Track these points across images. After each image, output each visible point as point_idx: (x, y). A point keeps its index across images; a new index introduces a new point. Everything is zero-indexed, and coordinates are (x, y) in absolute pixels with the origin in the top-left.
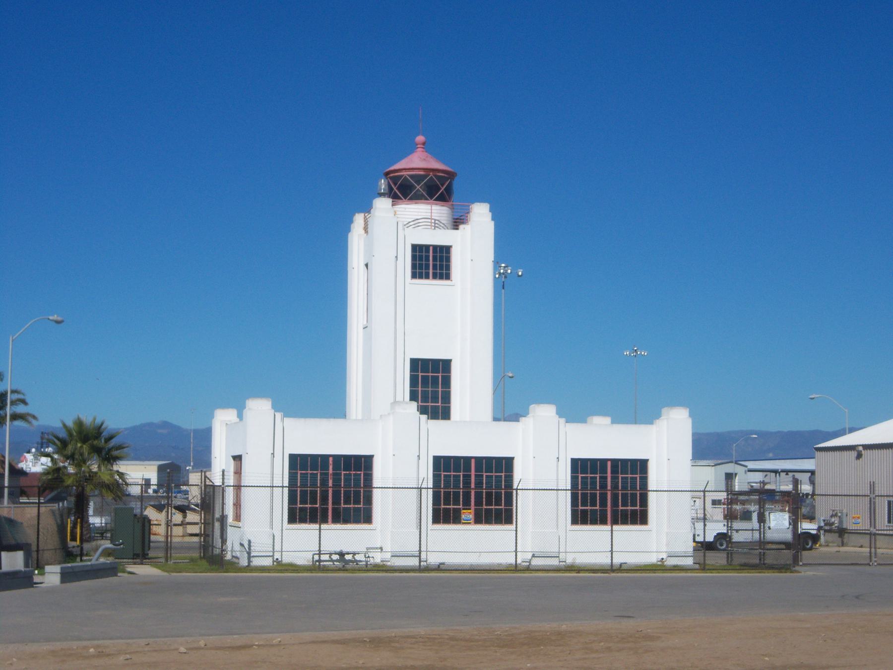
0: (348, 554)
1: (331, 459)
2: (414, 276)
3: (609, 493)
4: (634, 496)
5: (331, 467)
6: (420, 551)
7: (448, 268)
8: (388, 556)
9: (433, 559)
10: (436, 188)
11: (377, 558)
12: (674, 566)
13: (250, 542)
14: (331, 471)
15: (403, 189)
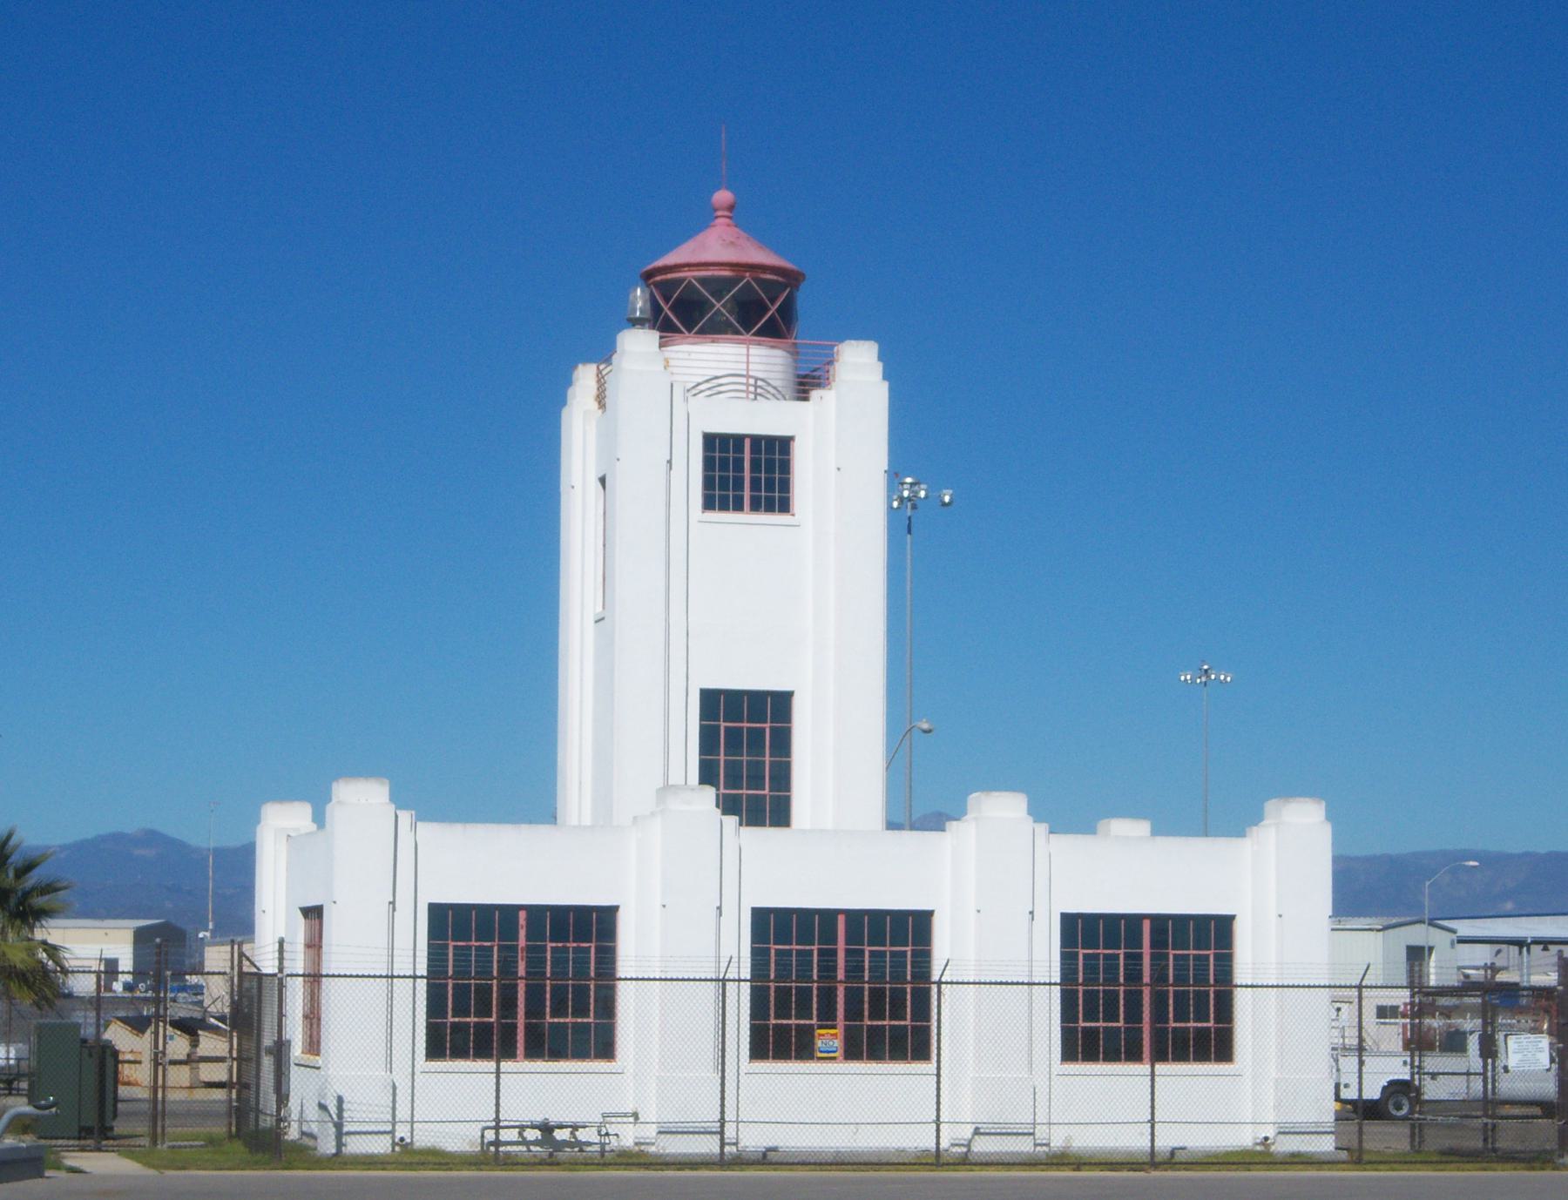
0: (561, 1127)
1: (522, 915)
2: (709, 504)
3: (1146, 992)
4: (1202, 998)
5: (522, 933)
6: (722, 1121)
7: (785, 486)
8: (650, 1132)
9: (752, 1139)
10: (757, 307)
11: (626, 1137)
12: (1293, 1155)
13: (340, 1100)
14: (522, 942)
15: (683, 311)
